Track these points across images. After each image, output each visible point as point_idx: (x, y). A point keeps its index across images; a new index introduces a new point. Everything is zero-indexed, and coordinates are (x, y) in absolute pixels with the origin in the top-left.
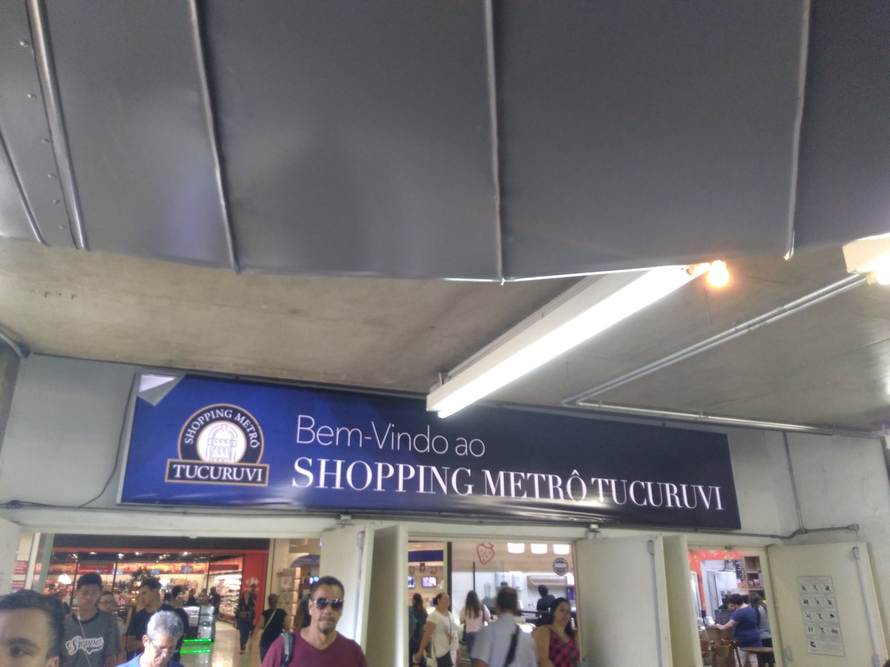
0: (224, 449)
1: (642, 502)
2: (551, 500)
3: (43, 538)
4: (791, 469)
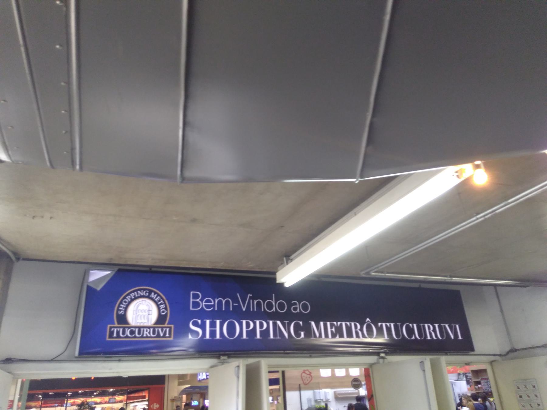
0: (144, 317)
1: (411, 337)
2: (354, 339)
3: (23, 383)
4: (502, 311)
